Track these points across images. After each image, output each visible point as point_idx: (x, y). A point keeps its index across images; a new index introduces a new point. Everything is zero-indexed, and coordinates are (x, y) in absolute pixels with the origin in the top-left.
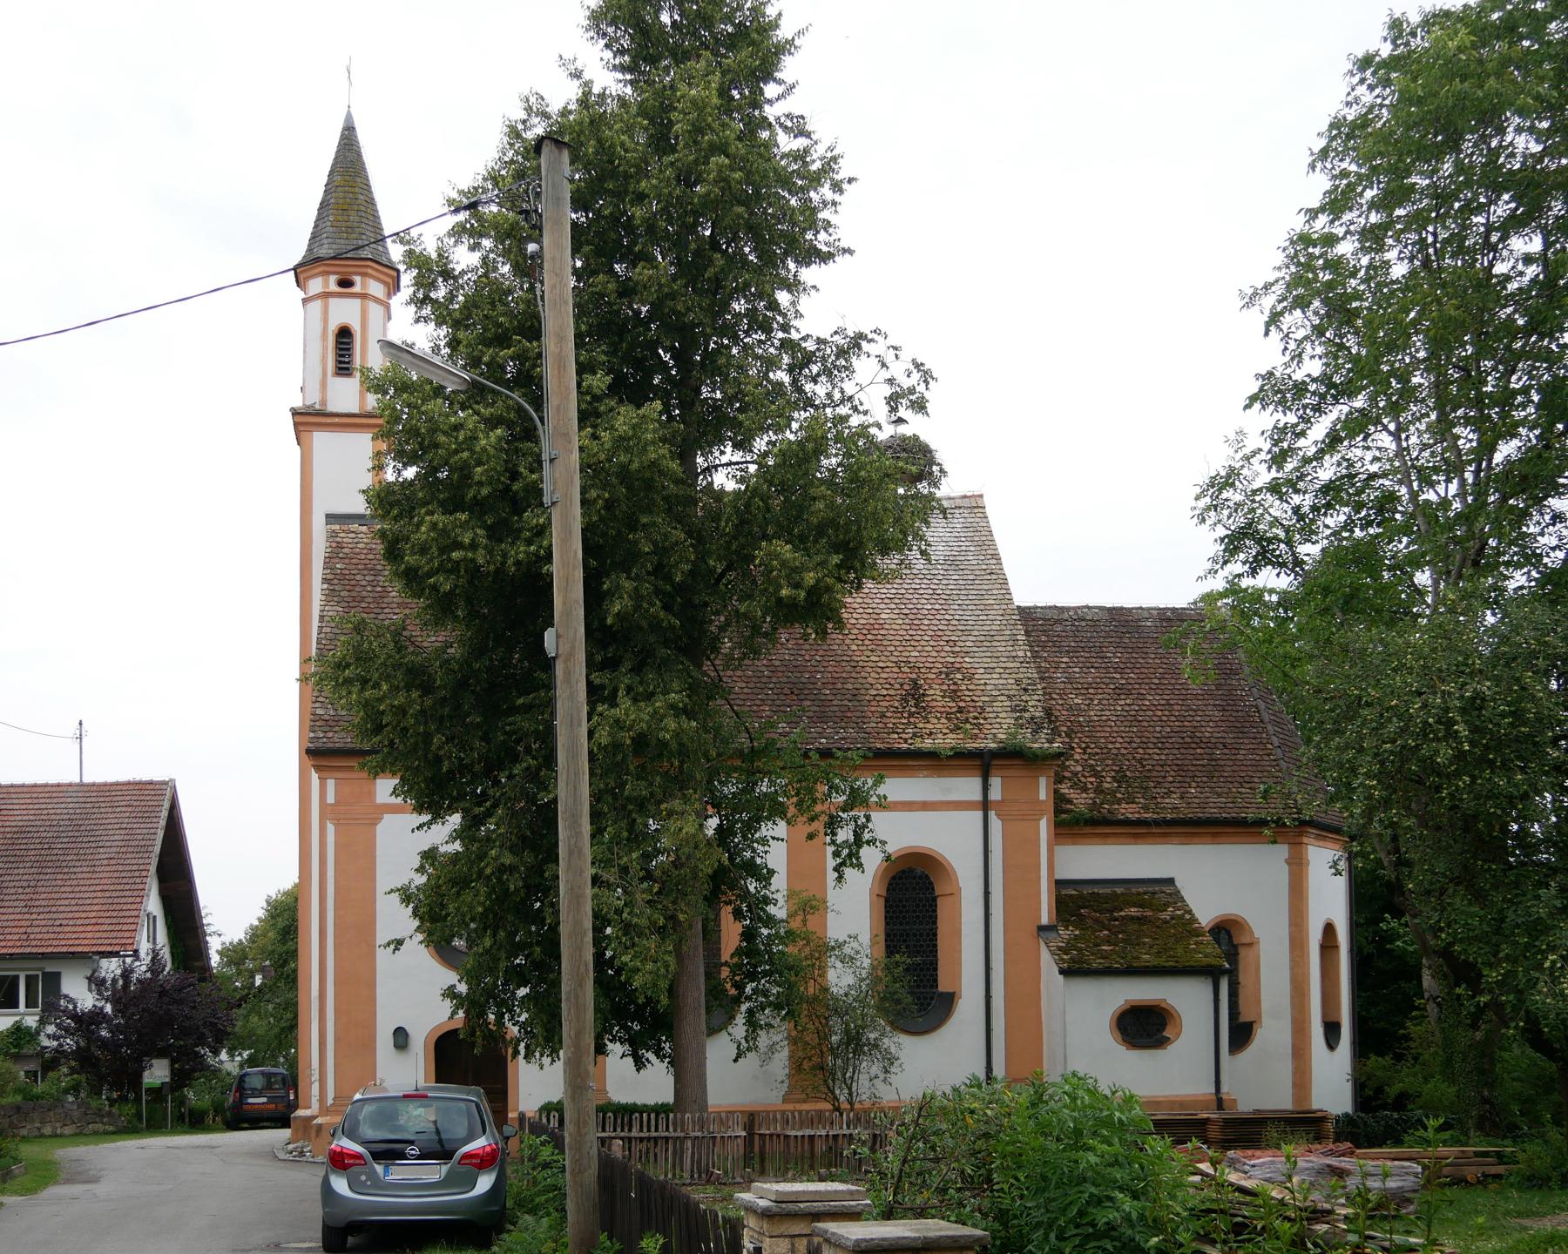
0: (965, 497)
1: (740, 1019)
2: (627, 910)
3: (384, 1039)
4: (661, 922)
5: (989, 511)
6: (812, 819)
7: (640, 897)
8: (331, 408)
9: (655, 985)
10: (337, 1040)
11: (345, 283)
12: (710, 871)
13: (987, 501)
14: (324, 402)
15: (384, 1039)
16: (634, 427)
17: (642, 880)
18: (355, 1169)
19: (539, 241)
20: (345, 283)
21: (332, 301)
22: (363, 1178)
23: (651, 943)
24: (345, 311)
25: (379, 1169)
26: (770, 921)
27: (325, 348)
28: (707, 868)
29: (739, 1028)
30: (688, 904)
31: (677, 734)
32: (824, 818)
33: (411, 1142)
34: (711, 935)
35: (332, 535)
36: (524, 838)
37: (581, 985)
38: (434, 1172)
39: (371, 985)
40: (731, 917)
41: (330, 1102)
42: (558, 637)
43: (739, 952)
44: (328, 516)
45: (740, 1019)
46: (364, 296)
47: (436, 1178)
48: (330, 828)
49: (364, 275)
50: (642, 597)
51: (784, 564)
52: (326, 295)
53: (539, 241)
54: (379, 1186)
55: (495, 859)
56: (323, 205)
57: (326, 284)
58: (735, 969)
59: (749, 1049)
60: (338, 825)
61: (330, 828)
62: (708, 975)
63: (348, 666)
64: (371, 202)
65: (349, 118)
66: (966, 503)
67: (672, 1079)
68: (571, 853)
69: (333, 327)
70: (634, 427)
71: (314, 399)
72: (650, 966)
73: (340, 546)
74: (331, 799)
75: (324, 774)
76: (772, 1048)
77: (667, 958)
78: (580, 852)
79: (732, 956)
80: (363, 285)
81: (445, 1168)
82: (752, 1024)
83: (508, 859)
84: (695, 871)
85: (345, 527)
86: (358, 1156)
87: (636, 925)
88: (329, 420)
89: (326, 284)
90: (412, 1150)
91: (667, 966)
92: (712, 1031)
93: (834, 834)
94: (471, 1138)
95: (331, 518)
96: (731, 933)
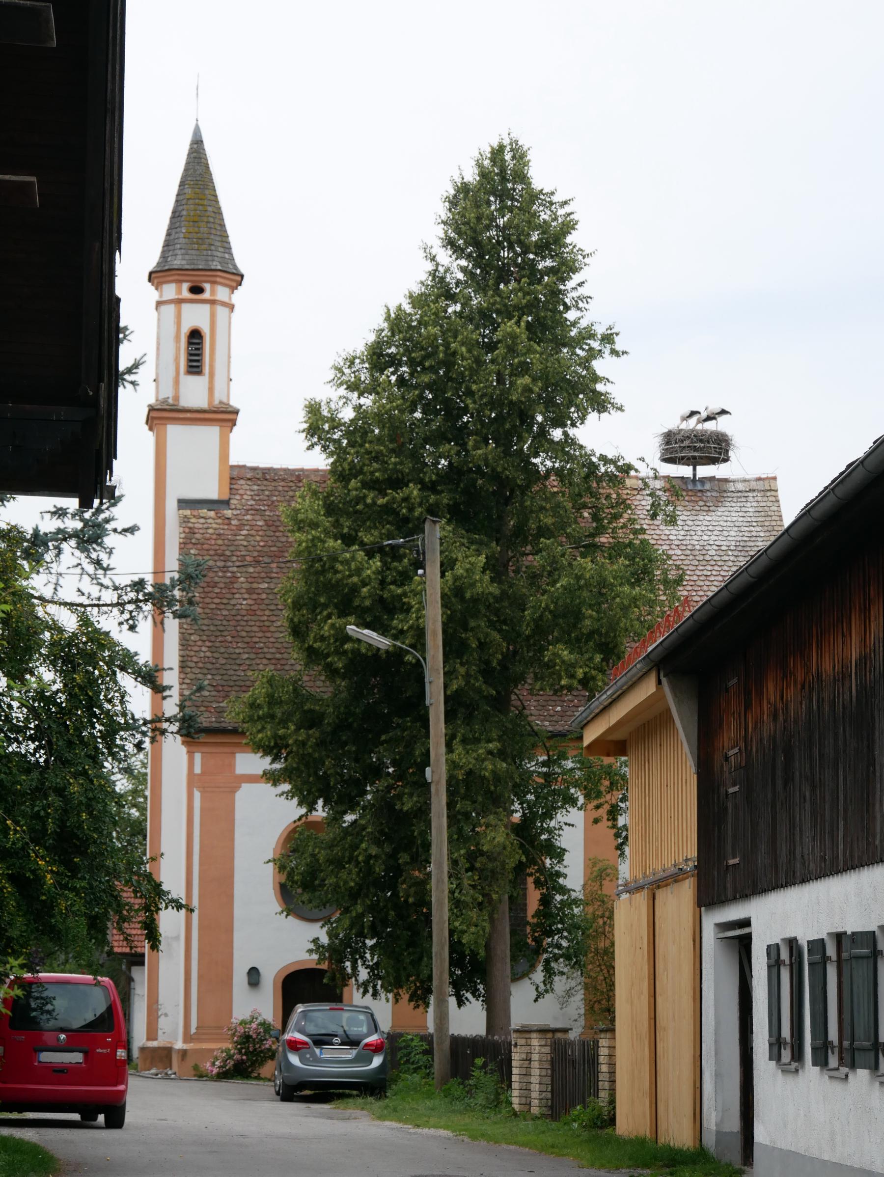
0: (759, 479)
1: (540, 968)
2: (458, 891)
3: (240, 978)
4: (480, 899)
5: (780, 494)
6: (597, 807)
7: (466, 882)
8: (185, 403)
9: (476, 942)
10: (200, 977)
11: (196, 290)
12: (513, 865)
13: (780, 485)
14: (177, 398)
15: (240, 978)
16: (467, 570)
17: (467, 871)
18: (303, 1051)
19: (423, 568)
20: (196, 290)
21: (185, 307)
22: (308, 1056)
23: (474, 914)
24: (196, 316)
25: (317, 1051)
26: (563, 890)
27: (178, 349)
28: (511, 863)
29: (538, 976)
30: (499, 886)
31: (494, 772)
32: (607, 807)
33: (336, 1036)
34: (517, 904)
35: (185, 520)
36: (382, 832)
37: (443, 948)
38: (351, 1054)
39: (230, 930)
40: (533, 886)
41: (193, 1030)
42: (433, 772)
43: (537, 914)
44: (180, 501)
45: (540, 968)
46: (213, 302)
47: (350, 1057)
48: (197, 795)
49: (213, 283)
50: (471, 676)
51: (563, 662)
52: (179, 302)
53: (423, 568)
54: (317, 1061)
55: (366, 850)
56: (176, 215)
57: (179, 291)
58: (534, 927)
59: (546, 991)
60: (203, 793)
61: (197, 795)
62: (513, 933)
63: (259, 707)
64: (218, 212)
65: (197, 132)
66: (760, 486)
67: (485, 1013)
68: (438, 882)
69: (185, 330)
70: (467, 570)
71: (167, 392)
72: (473, 929)
73: (192, 531)
74: (198, 770)
75: (193, 749)
76: (569, 993)
77: (484, 924)
78: (443, 882)
79: (533, 917)
80: (213, 292)
81: (354, 1052)
82: (549, 972)
83: (374, 850)
84: (503, 864)
85: (195, 513)
86: (306, 1043)
87: (464, 901)
88: (181, 415)
89: (179, 291)
90: (336, 1040)
91: (484, 930)
92: (517, 978)
93: (615, 819)
94: (369, 1034)
95: (183, 503)
96: (533, 898)
